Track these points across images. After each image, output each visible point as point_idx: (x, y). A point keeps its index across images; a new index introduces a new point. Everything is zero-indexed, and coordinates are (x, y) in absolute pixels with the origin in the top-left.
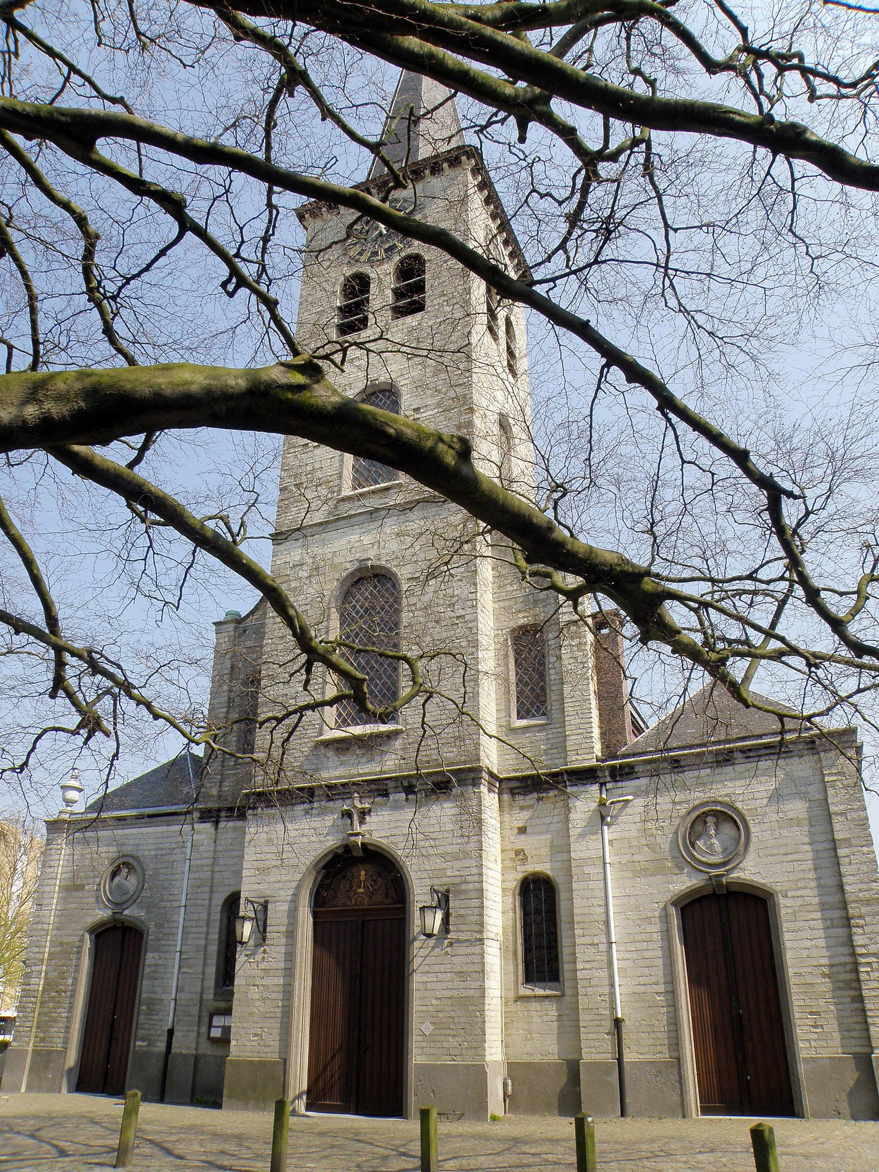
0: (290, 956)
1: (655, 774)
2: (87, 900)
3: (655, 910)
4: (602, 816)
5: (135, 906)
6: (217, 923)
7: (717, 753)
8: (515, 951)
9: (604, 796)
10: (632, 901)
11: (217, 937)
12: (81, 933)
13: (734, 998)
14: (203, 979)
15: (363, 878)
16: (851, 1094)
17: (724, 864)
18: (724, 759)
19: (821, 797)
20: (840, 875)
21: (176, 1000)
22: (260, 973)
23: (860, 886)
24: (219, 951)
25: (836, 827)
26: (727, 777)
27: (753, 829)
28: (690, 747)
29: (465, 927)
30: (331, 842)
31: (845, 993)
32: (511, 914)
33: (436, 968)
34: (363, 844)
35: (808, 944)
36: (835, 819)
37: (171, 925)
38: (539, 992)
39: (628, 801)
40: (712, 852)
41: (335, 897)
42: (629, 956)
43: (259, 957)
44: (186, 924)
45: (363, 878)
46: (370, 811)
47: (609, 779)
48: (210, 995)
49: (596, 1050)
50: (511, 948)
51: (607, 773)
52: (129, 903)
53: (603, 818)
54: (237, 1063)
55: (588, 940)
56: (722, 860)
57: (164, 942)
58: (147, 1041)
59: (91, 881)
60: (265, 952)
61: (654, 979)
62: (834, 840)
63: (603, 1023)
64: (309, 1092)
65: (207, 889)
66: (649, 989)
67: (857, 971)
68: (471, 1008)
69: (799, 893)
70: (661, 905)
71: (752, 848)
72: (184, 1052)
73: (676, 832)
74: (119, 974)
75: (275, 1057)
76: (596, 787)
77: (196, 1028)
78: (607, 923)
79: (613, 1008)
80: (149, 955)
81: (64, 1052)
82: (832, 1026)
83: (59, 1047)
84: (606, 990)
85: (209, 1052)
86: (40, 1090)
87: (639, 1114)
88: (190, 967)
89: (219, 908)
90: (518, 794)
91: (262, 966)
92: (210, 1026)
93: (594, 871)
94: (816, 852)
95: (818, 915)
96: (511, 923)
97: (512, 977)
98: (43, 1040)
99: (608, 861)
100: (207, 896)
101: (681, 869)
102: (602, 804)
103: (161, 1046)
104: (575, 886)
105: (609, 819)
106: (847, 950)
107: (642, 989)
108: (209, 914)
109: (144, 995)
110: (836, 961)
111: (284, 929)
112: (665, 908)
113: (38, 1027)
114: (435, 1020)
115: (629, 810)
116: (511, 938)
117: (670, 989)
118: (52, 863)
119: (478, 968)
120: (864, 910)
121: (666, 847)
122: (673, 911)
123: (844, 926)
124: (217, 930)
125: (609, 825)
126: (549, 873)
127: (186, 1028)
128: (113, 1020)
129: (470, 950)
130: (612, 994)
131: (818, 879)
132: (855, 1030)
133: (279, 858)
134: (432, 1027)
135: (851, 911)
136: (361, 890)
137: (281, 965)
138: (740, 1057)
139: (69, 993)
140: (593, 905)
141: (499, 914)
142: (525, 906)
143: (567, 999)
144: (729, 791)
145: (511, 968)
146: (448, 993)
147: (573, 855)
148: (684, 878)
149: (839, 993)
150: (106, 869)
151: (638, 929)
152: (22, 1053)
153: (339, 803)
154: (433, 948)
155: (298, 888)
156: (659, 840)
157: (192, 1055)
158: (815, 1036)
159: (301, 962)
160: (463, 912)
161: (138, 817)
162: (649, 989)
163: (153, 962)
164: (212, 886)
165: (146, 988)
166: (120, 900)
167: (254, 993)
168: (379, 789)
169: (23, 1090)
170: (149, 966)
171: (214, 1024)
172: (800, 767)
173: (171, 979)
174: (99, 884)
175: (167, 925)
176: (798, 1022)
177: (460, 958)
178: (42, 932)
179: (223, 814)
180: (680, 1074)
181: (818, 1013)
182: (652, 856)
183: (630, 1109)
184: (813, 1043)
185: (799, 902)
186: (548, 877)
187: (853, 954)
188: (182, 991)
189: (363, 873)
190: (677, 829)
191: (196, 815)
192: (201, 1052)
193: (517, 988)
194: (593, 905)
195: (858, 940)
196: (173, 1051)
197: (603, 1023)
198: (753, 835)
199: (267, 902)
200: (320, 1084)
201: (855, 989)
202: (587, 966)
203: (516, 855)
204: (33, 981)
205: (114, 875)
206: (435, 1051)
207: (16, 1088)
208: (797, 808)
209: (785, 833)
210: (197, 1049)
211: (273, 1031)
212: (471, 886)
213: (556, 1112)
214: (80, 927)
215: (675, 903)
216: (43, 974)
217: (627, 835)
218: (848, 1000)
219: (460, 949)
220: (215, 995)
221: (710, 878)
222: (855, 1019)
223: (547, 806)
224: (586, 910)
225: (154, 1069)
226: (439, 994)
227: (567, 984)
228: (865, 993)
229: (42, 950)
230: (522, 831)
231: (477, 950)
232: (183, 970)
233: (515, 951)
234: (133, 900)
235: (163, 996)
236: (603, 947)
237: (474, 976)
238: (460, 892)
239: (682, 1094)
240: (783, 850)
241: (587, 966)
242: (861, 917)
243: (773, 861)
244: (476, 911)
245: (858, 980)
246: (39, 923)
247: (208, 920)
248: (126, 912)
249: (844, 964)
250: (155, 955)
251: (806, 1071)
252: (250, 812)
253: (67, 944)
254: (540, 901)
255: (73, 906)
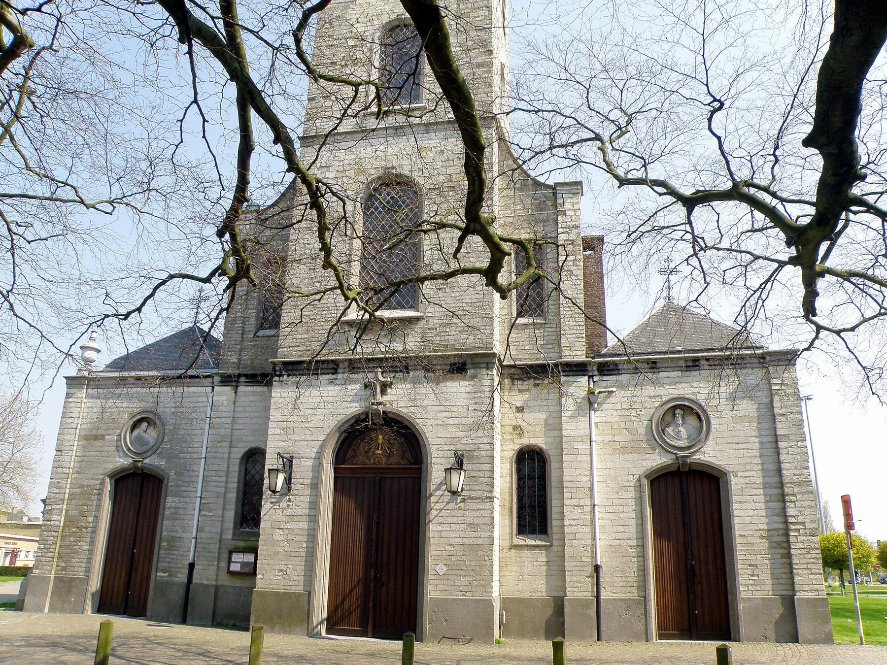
0: (314, 505)
1: (636, 371)
2: (106, 449)
3: (631, 481)
4: (591, 402)
5: (155, 456)
6: (236, 474)
7: (686, 360)
8: (511, 508)
9: (592, 386)
10: (612, 472)
11: (235, 485)
12: (102, 477)
13: (689, 552)
14: (222, 521)
15: (380, 441)
16: (776, 623)
17: (689, 448)
18: (693, 364)
19: (768, 400)
20: (779, 462)
21: (196, 538)
22: (284, 518)
23: (795, 471)
24: (237, 497)
25: (779, 425)
26: (695, 379)
27: (713, 422)
28: (659, 353)
29: (477, 487)
30: (354, 408)
31: (777, 551)
32: (508, 478)
33: (450, 520)
34: (384, 412)
35: (751, 513)
36: (778, 419)
37: (191, 473)
38: (531, 542)
39: (613, 392)
40: (679, 438)
41: (354, 457)
42: (607, 516)
43: (284, 505)
44: (206, 473)
45: (380, 441)
46: (391, 384)
47: (596, 373)
48: (229, 535)
49: (578, 588)
50: (507, 505)
51: (595, 368)
52: (150, 452)
53: (591, 404)
54: (263, 594)
55: (574, 502)
56: (687, 444)
57: (184, 489)
58: (168, 570)
59: (111, 432)
60: (289, 500)
61: (627, 535)
62: (776, 435)
63: (585, 568)
64: (328, 619)
65: (227, 444)
66: (623, 543)
67: (788, 535)
68: (480, 553)
69: (746, 474)
70: (636, 477)
71: (711, 437)
72: (204, 582)
73: (651, 420)
74: (138, 515)
75: (300, 589)
76: (586, 378)
77: (216, 563)
78: (591, 489)
79: (594, 556)
80: (170, 499)
81: (87, 580)
82: (766, 574)
83: (82, 575)
84: (589, 542)
85: (228, 583)
86: (63, 610)
87: (611, 639)
88: (211, 511)
89: (238, 461)
90: (518, 379)
91: (286, 512)
92: (230, 561)
93: (583, 447)
94: (761, 443)
95: (761, 492)
96: (508, 485)
97: (507, 530)
98: (64, 569)
99: (594, 439)
100: (227, 450)
101: (654, 449)
102: (591, 392)
103: (182, 577)
104: (565, 458)
105: (596, 405)
106: (781, 519)
107: (618, 543)
108: (228, 466)
109: (165, 533)
110: (772, 527)
111: (309, 481)
112: (639, 480)
113: (60, 557)
114: (448, 563)
115: (612, 399)
116: (507, 498)
117: (641, 544)
118: (72, 415)
119: (488, 521)
120: (796, 489)
121: (642, 431)
122: (645, 482)
123: (779, 501)
124: (236, 480)
125: (595, 410)
126: (544, 447)
127: (206, 563)
128: (133, 553)
129: (480, 506)
130: (594, 545)
131: (762, 464)
132: (782, 578)
133: (305, 421)
134: (445, 568)
135: (786, 490)
136: (380, 452)
137: (307, 512)
138: (691, 597)
139: (90, 530)
140: (580, 474)
141: (503, 479)
142: (519, 471)
143: (555, 548)
144: (696, 391)
145: (507, 522)
146: (460, 541)
147: (564, 432)
148: (656, 456)
149: (773, 551)
150: (126, 420)
151: (616, 496)
152: (45, 580)
153: (361, 376)
154: (448, 503)
155: (322, 447)
156: (636, 425)
157: (213, 585)
158: (752, 582)
159: (324, 511)
160: (475, 474)
161: (163, 378)
162: (623, 543)
163: (173, 505)
164: (231, 442)
165: (166, 527)
166: (141, 450)
167: (279, 535)
168: (401, 366)
169: (46, 610)
170: (169, 508)
171: (233, 560)
172: (753, 376)
173: (192, 522)
174: (120, 435)
175: (186, 473)
176: (740, 572)
177: (472, 512)
178: (63, 475)
179: (243, 379)
180: (645, 609)
181: (756, 565)
182: (630, 438)
183: (603, 635)
184: (750, 588)
185: (747, 481)
186: (541, 449)
187: (786, 522)
188: (203, 531)
189: (381, 437)
190: (652, 417)
191: (217, 379)
192: (220, 583)
193: (512, 538)
194: (580, 474)
195: (791, 512)
196: (194, 581)
197: (585, 568)
198: (713, 427)
199: (292, 457)
200: (339, 613)
201: (785, 548)
202: (573, 523)
203: (514, 430)
204: (54, 517)
205: (134, 427)
206: (448, 588)
207: (39, 609)
208: (748, 408)
209: (738, 427)
210: (216, 581)
211: (297, 568)
212: (483, 453)
213: (543, 637)
214: (101, 472)
215: (647, 477)
216: (64, 512)
217: (609, 419)
218: (779, 556)
219: (471, 505)
220: (234, 535)
221: (677, 458)
222: (782, 571)
223: (546, 390)
224: (574, 478)
225: (177, 597)
226: (452, 541)
227: (555, 537)
228: (793, 551)
229: (63, 490)
230: (520, 410)
231: (487, 506)
232: (203, 513)
233: (511, 508)
234: (153, 450)
235: (184, 535)
236: (588, 509)
237: (484, 527)
238: (473, 457)
239: (646, 624)
240: (735, 440)
241: (573, 523)
242: (794, 495)
243: (731, 447)
244: (487, 474)
245: (788, 542)
246: (59, 467)
247: (228, 471)
248: (147, 461)
249: (777, 530)
250: (175, 499)
251: (744, 607)
252: (276, 378)
253: (88, 486)
254: (533, 468)
255: (93, 453)
